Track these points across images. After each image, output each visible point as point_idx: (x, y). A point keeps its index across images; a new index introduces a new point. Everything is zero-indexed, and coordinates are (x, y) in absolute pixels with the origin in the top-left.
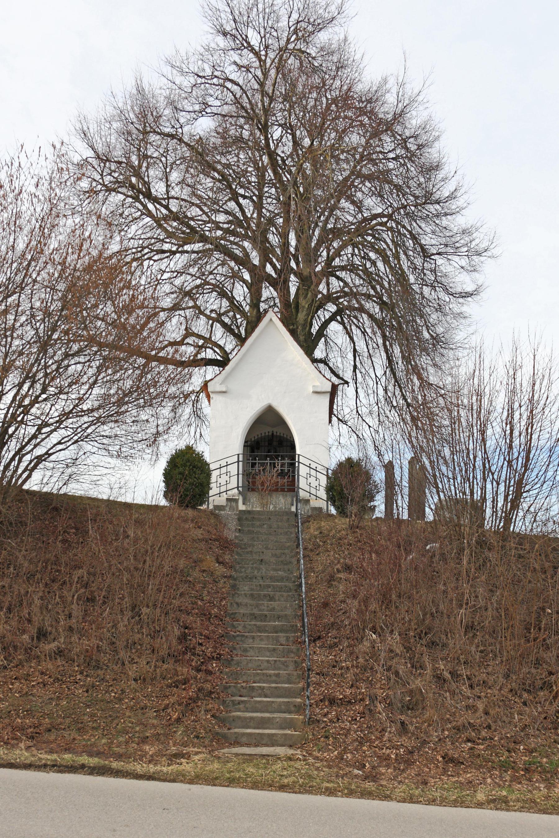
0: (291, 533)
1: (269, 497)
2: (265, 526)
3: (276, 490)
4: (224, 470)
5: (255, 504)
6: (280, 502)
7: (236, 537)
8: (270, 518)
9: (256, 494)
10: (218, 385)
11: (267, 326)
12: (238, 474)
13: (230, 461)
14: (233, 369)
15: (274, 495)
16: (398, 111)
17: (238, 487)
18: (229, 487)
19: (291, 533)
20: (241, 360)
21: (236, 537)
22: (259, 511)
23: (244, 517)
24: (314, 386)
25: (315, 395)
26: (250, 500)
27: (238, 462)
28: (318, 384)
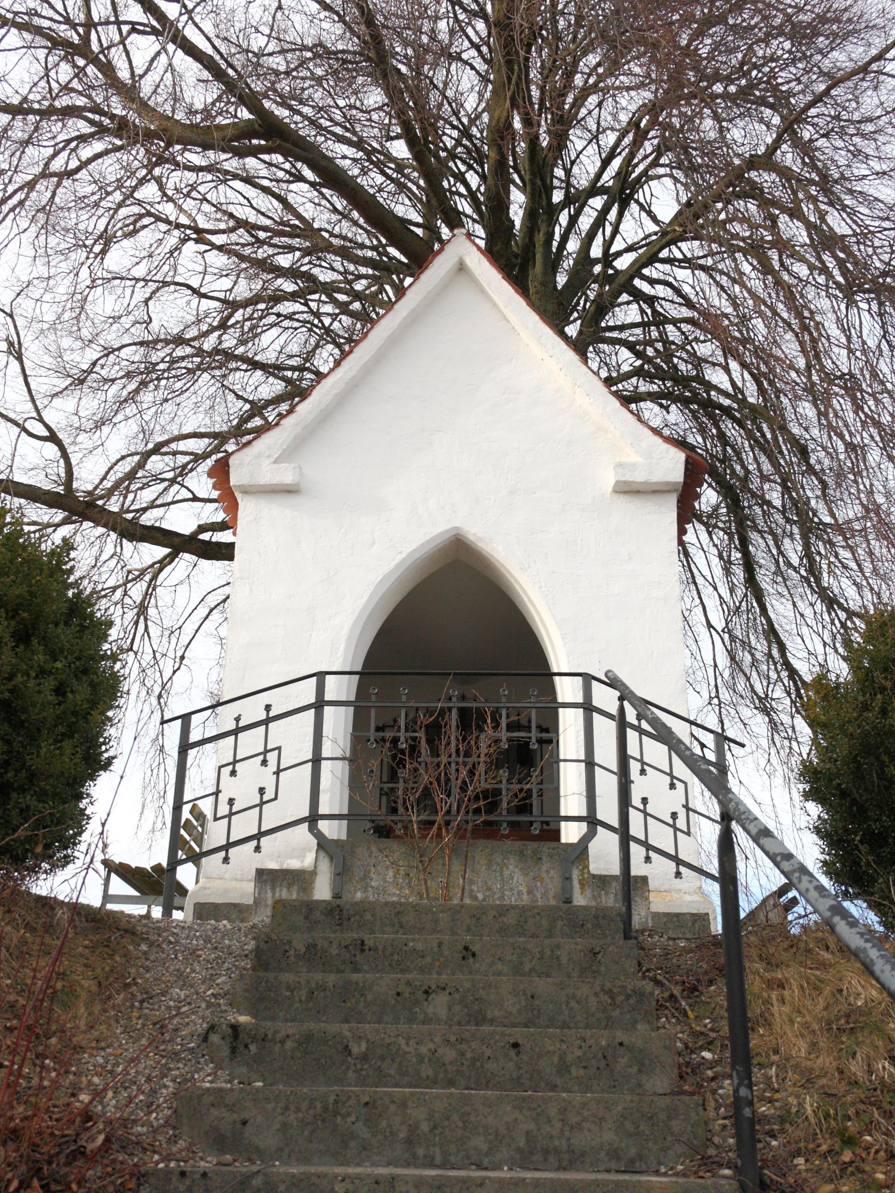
0: (643, 1062)
1: (457, 866)
2: (439, 1005)
3: (489, 831)
4: (251, 742)
5: (387, 880)
6: (506, 880)
7: (189, 1103)
8: (468, 952)
9: (396, 849)
10: (266, 463)
11: (446, 286)
12: (316, 760)
13: (281, 701)
14: (325, 417)
15: (481, 850)
16: (469, 862)
17: (313, 819)
18: (273, 816)
19: (643, 1062)
20: (354, 387)
21: (189, 1103)
22: (398, 911)
23: (299, 943)
24: (619, 465)
25: (624, 500)
26: (366, 877)
27: (319, 705)
28: (632, 457)
